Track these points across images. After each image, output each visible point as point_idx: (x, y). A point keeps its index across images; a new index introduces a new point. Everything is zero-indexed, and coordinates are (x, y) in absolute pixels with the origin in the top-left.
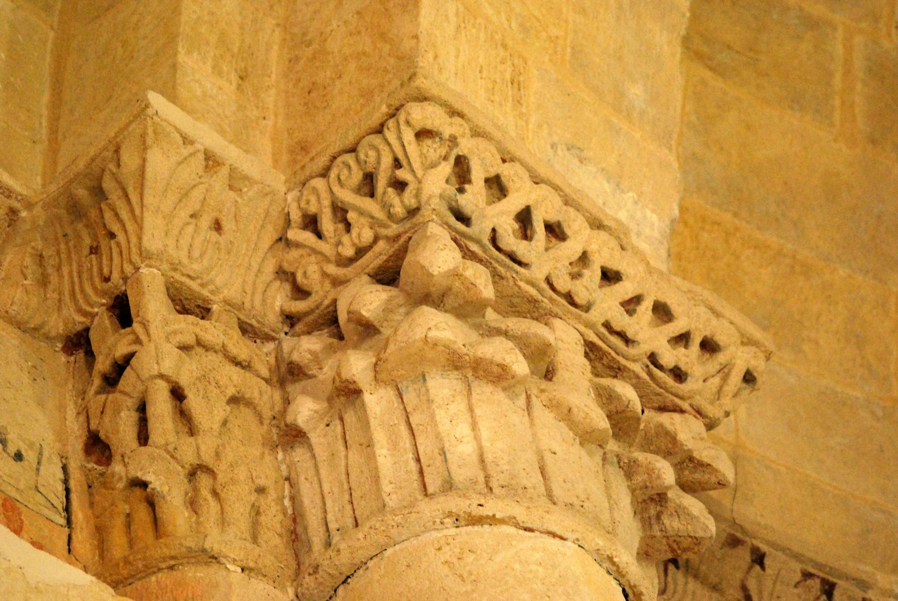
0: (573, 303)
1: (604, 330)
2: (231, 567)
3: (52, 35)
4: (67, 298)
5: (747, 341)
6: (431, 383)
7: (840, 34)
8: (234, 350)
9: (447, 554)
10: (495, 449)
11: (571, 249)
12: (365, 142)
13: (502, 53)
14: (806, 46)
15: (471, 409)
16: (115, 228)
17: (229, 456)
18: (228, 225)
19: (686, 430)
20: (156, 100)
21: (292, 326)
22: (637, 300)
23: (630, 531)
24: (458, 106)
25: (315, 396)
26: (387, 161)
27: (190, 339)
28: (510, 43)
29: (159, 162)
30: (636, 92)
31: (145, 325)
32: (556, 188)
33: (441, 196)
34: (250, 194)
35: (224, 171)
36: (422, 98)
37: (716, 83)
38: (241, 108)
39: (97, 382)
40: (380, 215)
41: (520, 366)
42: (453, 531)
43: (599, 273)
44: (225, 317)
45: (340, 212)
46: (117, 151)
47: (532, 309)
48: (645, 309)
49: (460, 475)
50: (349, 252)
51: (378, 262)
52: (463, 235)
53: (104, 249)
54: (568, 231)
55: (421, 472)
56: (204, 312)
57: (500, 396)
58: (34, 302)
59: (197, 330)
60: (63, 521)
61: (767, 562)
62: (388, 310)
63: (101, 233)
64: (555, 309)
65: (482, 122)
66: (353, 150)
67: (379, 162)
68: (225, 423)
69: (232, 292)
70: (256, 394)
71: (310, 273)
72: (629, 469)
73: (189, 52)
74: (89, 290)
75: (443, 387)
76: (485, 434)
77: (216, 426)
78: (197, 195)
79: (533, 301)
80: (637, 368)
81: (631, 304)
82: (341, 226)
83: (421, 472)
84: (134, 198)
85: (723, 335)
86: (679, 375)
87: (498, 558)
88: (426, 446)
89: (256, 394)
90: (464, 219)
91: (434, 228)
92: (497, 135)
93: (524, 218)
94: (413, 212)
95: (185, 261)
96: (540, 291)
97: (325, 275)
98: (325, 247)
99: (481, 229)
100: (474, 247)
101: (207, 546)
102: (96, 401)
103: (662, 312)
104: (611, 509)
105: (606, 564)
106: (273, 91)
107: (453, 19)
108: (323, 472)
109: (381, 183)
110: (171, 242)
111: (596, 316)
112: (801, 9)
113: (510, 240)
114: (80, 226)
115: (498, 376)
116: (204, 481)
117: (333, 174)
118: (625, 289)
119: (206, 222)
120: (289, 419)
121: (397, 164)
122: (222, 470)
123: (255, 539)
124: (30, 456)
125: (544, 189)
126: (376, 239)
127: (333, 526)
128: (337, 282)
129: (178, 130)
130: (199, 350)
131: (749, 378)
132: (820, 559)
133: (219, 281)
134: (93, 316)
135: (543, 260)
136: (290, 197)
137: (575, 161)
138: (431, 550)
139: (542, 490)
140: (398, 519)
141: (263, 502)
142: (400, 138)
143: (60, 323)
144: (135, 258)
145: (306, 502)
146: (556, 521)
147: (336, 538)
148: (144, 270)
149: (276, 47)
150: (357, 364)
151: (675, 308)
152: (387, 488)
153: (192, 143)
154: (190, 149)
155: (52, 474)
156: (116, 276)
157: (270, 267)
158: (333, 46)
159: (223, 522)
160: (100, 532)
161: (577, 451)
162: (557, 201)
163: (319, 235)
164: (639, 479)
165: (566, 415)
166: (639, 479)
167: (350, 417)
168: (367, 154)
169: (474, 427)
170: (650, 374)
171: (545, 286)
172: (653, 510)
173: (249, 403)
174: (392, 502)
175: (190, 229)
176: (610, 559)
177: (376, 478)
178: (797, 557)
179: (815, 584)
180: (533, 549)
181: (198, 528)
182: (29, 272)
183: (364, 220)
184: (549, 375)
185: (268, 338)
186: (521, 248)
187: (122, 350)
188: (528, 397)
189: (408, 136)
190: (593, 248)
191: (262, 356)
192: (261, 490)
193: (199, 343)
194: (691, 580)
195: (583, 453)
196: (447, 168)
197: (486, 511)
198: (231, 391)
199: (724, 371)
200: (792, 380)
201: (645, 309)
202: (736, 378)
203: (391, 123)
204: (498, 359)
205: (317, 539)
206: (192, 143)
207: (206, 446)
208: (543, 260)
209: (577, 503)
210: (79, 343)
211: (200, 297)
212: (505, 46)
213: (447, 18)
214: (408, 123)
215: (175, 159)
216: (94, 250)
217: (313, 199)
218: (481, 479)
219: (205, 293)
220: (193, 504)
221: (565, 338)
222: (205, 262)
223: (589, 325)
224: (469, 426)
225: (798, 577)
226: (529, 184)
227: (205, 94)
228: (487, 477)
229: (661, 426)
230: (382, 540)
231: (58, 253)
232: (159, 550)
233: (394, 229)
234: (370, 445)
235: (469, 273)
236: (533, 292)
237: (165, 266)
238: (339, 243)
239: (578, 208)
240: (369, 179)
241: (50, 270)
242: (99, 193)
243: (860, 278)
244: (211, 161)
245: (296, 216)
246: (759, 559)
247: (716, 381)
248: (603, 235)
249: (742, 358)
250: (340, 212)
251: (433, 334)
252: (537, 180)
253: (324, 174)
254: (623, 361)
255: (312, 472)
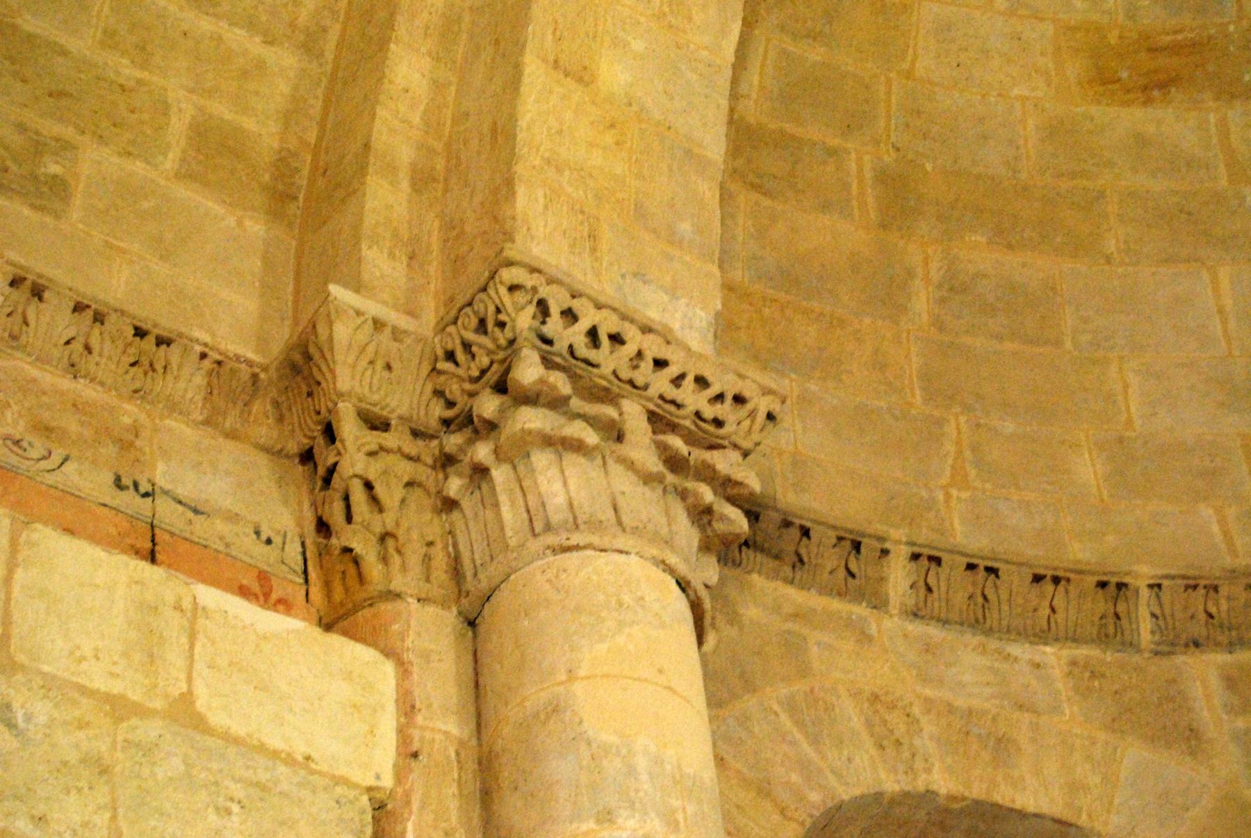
0: (635, 387)
1: (660, 402)
2: (410, 600)
3: (294, 243)
4: (297, 429)
5: (767, 392)
6: (533, 458)
7: (853, 156)
8: (406, 450)
9: (550, 574)
10: (581, 497)
11: (629, 349)
12: (477, 298)
13: (580, 217)
14: (831, 168)
15: (562, 472)
16: (319, 378)
17: (405, 524)
18: (396, 365)
19: (725, 462)
20: (335, 290)
21: (448, 426)
22: (682, 376)
23: (687, 534)
24: (535, 264)
25: (460, 475)
26: (491, 309)
27: (374, 447)
28: (586, 209)
29: (342, 332)
30: (685, 227)
31: (342, 441)
32: (614, 310)
33: (530, 328)
34: (409, 341)
35: (388, 331)
36: (510, 264)
37: (767, 202)
38: (411, 279)
39: (319, 483)
40: (490, 345)
41: (591, 437)
42: (552, 558)
43: (652, 363)
44: (400, 428)
45: (467, 346)
46: (314, 327)
47: (605, 396)
48: (689, 382)
49: (555, 518)
50: (476, 373)
51: (495, 378)
52: (549, 353)
53: (315, 392)
54: (626, 338)
55: (531, 520)
56: (385, 426)
57: (582, 460)
58: (275, 434)
59: (380, 440)
60: (302, 581)
61: (812, 533)
62: (502, 411)
63: (312, 382)
64: (622, 392)
65: (553, 272)
66: (470, 304)
67: (486, 308)
68: (403, 501)
69: (403, 410)
70: (424, 478)
71: (454, 390)
72: (683, 495)
73: (370, 247)
74: (309, 421)
75: (542, 459)
76: (572, 488)
77: (397, 504)
78: (371, 349)
79: (606, 390)
80: (687, 423)
81: (678, 381)
82: (469, 357)
83: (531, 520)
84: (328, 356)
85: (748, 390)
86: (718, 423)
87: (582, 574)
88: (533, 501)
89: (424, 478)
90: (548, 341)
91: (526, 352)
92: (567, 280)
93: (593, 333)
94: (512, 342)
95: (368, 395)
96: (609, 382)
97: (463, 391)
98: (460, 372)
99: (561, 346)
100: (558, 360)
101: (392, 587)
102: (320, 496)
103: (701, 382)
104: (669, 525)
105: (662, 566)
106: (435, 263)
107: (541, 200)
108: (471, 524)
109: (490, 325)
110: (357, 384)
111: (652, 392)
112: (824, 143)
113: (583, 351)
114: (299, 379)
115: (578, 447)
116: (390, 543)
117: (459, 322)
118: (673, 371)
119: (380, 364)
120: (444, 493)
121: (498, 311)
122: (401, 533)
123: (428, 580)
124: (277, 540)
125: (605, 312)
126: (492, 363)
127: (478, 562)
128: (472, 395)
129: (352, 308)
130: (383, 454)
131: (770, 417)
132: (849, 526)
133: (394, 404)
134: (314, 438)
135: (608, 360)
136: (436, 340)
137: (640, 284)
138: (538, 573)
139: (613, 520)
140: (515, 555)
141: (432, 551)
142: (497, 293)
143: (293, 447)
144: (334, 397)
145: (461, 547)
146: (622, 542)
147: (480, 569)
148: (340, 405)
149: (436, 233)
150: (483, 452)
151: (710, 379)
152: (509, 533)
153: (363, 314)
154: (362, 319)
155: (294, 550)
156: (323, 411)
157: (429, 388)
158: (468, 228)
159: (404, 569)
160: (327, 585)
161: (641, 489)
162: (615, 318)
163: (457, 364)
164: (690, 500)
165: (630, 465)
166: (690, 500)
167: (484, 486)
168: (479, 306)
169: (565, 484)
170: (697, 425)
171: (612, 378)
172: (705, 519)
173: (420, 485)
174: (513, 542)
175: (369, 373)
176: (663, 562)
177: (502, 529)
178: (834, 527)
179: (847, 544)
180: (607, 564)
181: (388, 578)
182: (270, 414)
183: (482, 351)
184: (620, 438)
185: (432, 437)
186: (592, 355)
187: (331, 460)
188: (604, 457)
189: (503, 291)
190: (645, 346)
191: (428, 450)
192: (430, 544)
193: (382, 448)
194: (759, 555)
195: (646, 489)
196: (531, 309)
197: (573, 542)
198: (406, 479)
199: (752, 414)
200: (835, 402)
201: (689, 382)
202: (761, 417)
203: (491, 284)
204: (576, 436)
205: (469, 575)
206: (363, 314)
207: (389, 519)
208: (608, 360)
209: (641, 526)
210: (307, 457)
211: (380, 417)
212: (582, 212)
213: (536, 200)
214: (501, 282)
215: (353, 326)
216: (310, 394)
217: (449, 340)
218: (571, 520)
219: (385, 413)
220: (385, 559)
221: (633, 413)
222: (382, 393)
223: (649, 399)
224: (559, 483)
225: (834, 541)
226: (592, 310)
227: (382, 276)
228: (575, 518)
229: (704, 462)
230: (507, 570)
231: (288, 399)
232: (360, 596)
233: (501, 355)
234: (496, 505)
235: (552, 379)
236: (604, 383)
237: (354, 400)
238: (469, 368)
239: (632, 321)
240: (482, 322)
241: (285, 411)
242: (308, 357)
243: (880, 323)
244: (378, 324)
245: (440, 353)
246: (806, 532)
247: (747, 423)
248: (651, 336)
249: (764, 405)
250: (467, 346)
251: (527, 426)
252: (599, 307)
253: (455, 322)
254: (676, 420)
255: (463, 528)
